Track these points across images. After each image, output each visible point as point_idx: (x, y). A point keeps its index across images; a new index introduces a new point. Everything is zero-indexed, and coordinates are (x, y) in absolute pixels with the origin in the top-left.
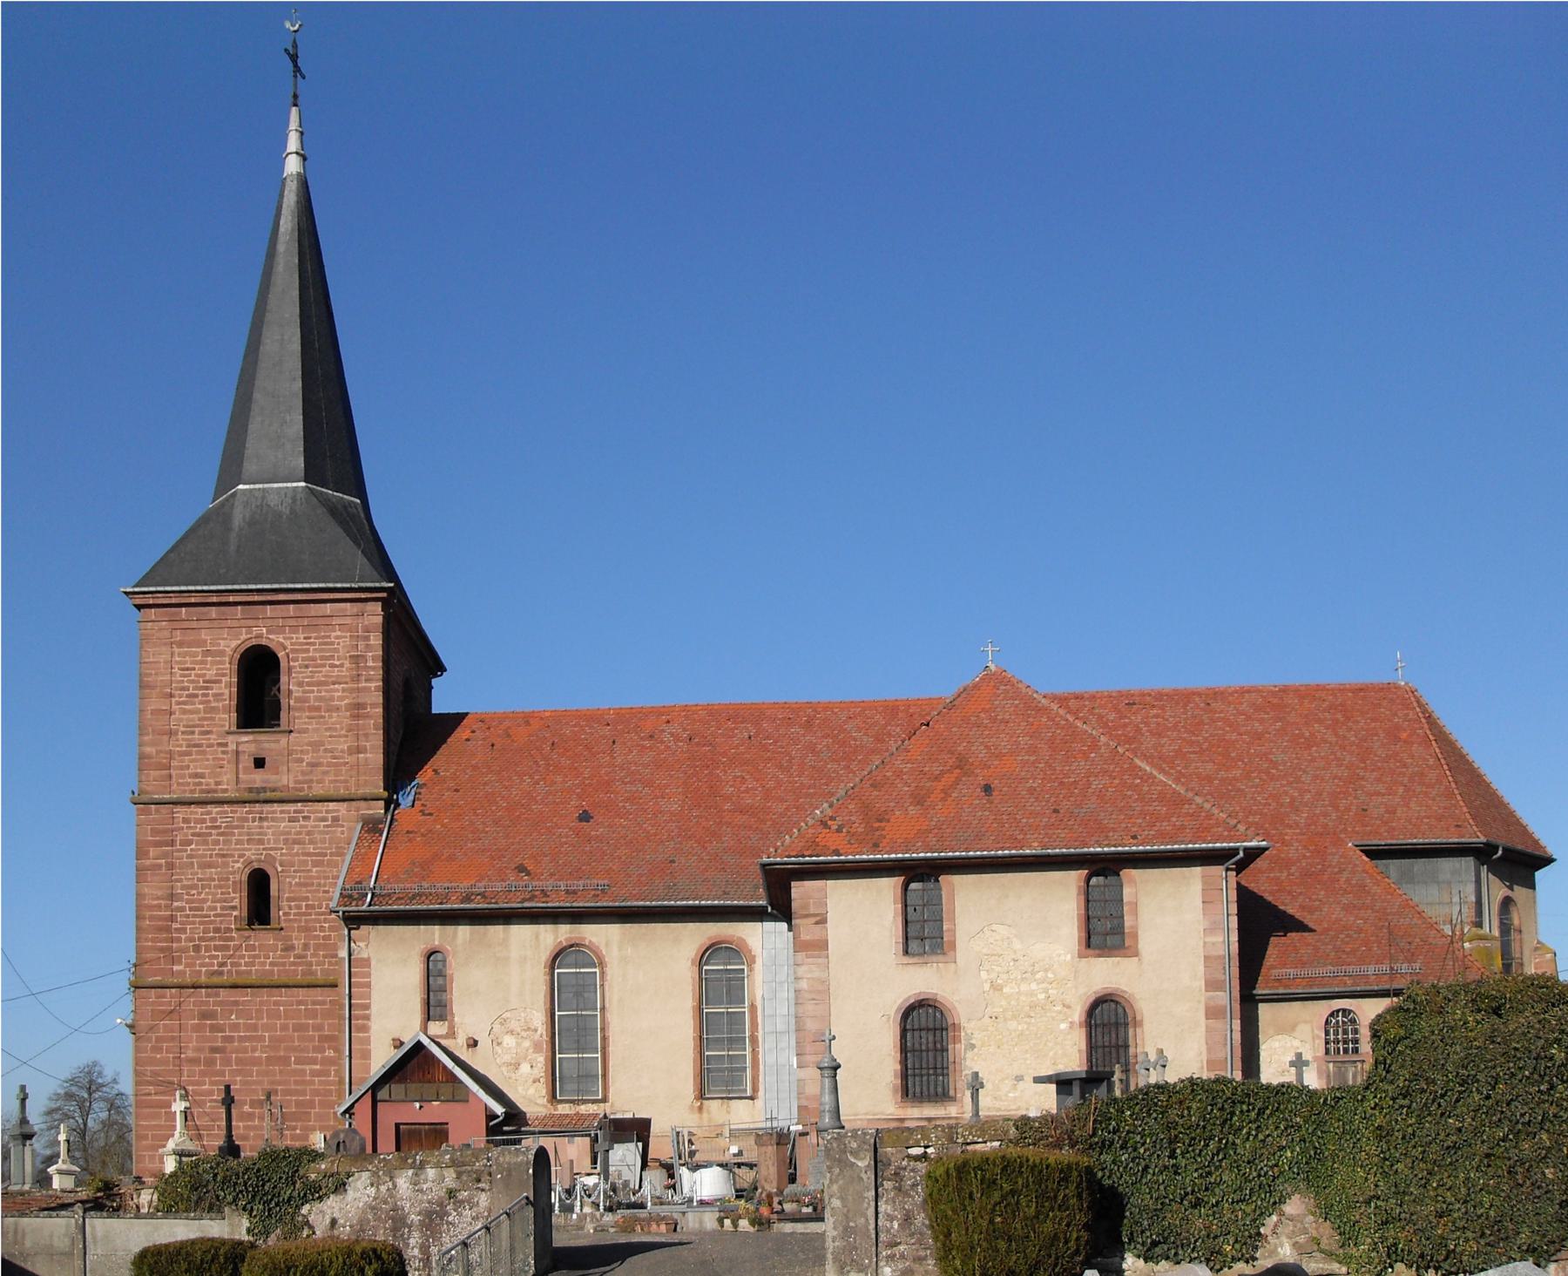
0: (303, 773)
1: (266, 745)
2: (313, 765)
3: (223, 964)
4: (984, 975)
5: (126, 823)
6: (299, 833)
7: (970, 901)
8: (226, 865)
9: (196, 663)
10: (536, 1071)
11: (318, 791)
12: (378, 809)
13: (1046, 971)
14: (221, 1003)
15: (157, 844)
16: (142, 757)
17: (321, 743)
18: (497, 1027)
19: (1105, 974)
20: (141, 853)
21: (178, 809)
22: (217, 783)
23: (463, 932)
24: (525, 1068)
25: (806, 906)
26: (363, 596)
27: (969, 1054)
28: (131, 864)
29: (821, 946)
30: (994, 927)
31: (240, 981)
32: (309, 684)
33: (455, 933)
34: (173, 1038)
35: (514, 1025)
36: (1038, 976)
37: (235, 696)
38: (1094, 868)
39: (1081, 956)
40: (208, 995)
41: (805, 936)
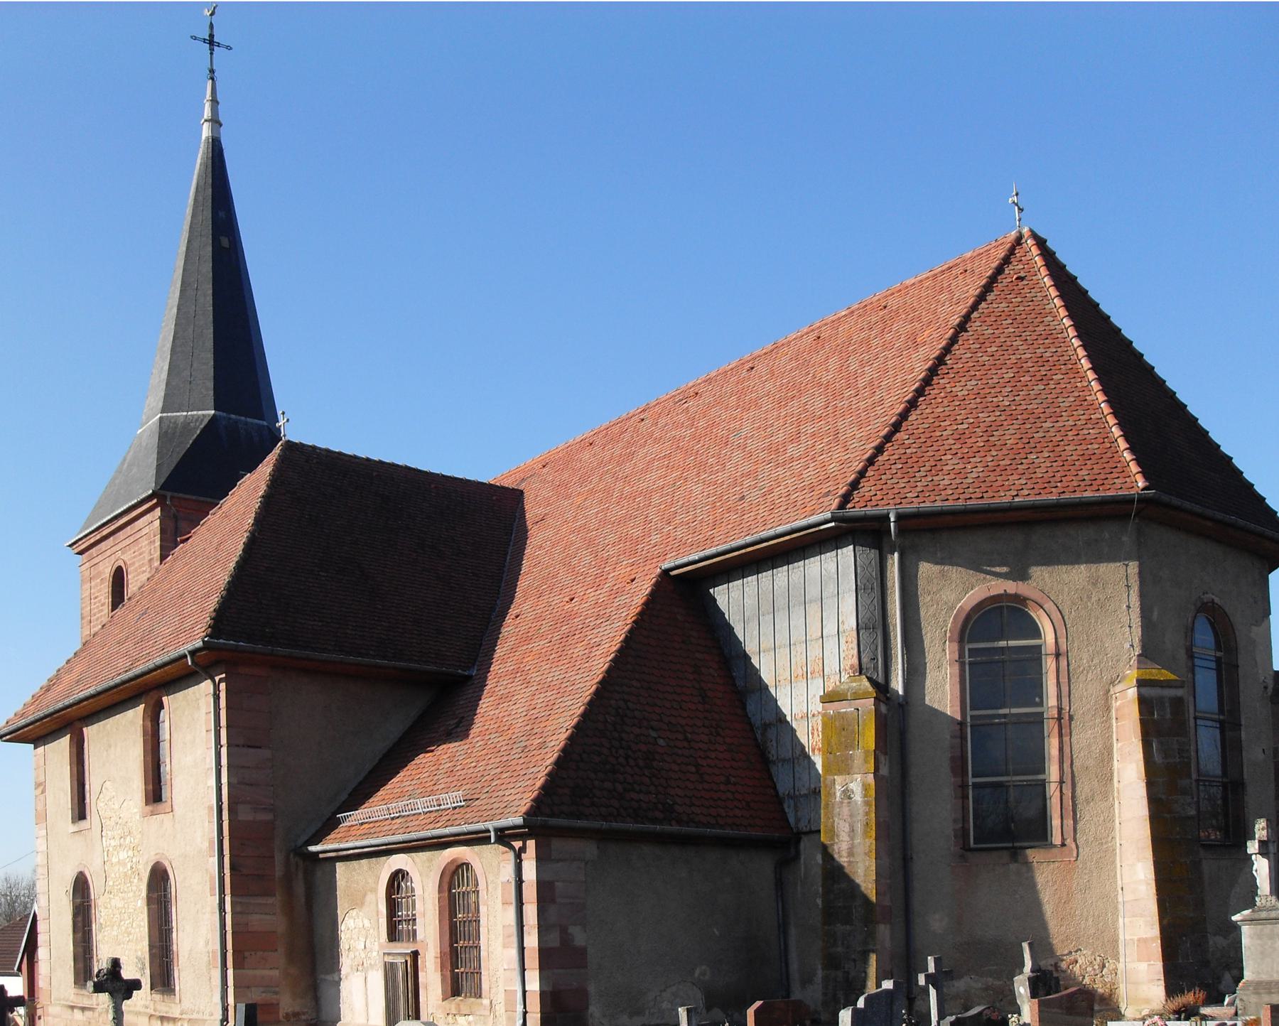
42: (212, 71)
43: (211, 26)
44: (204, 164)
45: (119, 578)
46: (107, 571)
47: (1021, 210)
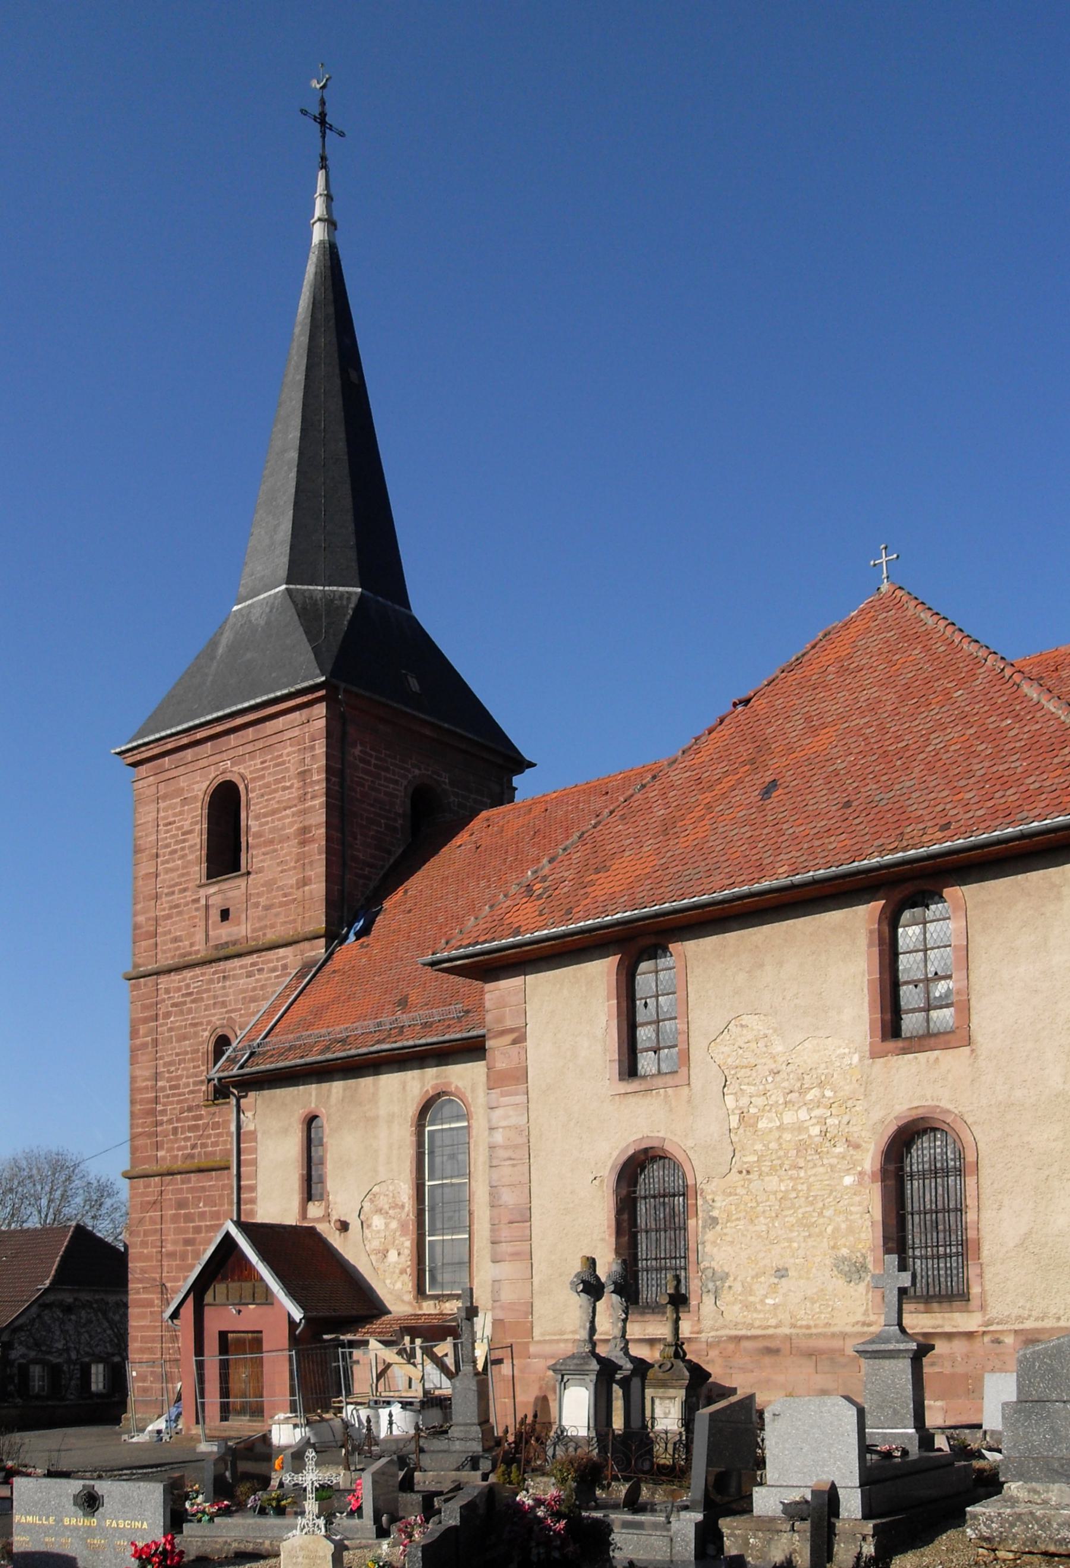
0: (260, 919)
1: (230, 894)
2: (267, 908)
3: (194, 1147)
4: (730, 1100)
5: (118, 1003)
6: (254, 989)
7: (707, 974)
8: (196, 1034)
9: (175, 815)
10: (403, 1258)
11: (271, 936)
12: (318, 950)
13: (821, 1085)
14: (191, 1190)
15: (146, 1020)
16: (136, 927)
17: (273, 881)
18: (367, 1205)
19: (912, 1084)
20: (134, 1034)
21: (163, 979)
22: (192, 945)
23: (337, 1087)
24: (393, 1256)
25: (500, 1020)
26: (310, 697)
27: (710, 1235)
28: (124, 1043)
29: (519, 1076)
30: (746, 1019)
31: (204, 1164)
32: (265, 815)
33: (329, 1091)
34: (156, 1231)
35: (383, 1202)
36: (809, 1096)
37: (205, 844)
38: (898, 894)
39: (875, 1054)
40: (183, 1183)
41: (501, 1064)
42: (323, 158)
43: (323, 103)
44: (315, 304)
45: (225, 805)
46: (199, 786)
47: (900, 588)
